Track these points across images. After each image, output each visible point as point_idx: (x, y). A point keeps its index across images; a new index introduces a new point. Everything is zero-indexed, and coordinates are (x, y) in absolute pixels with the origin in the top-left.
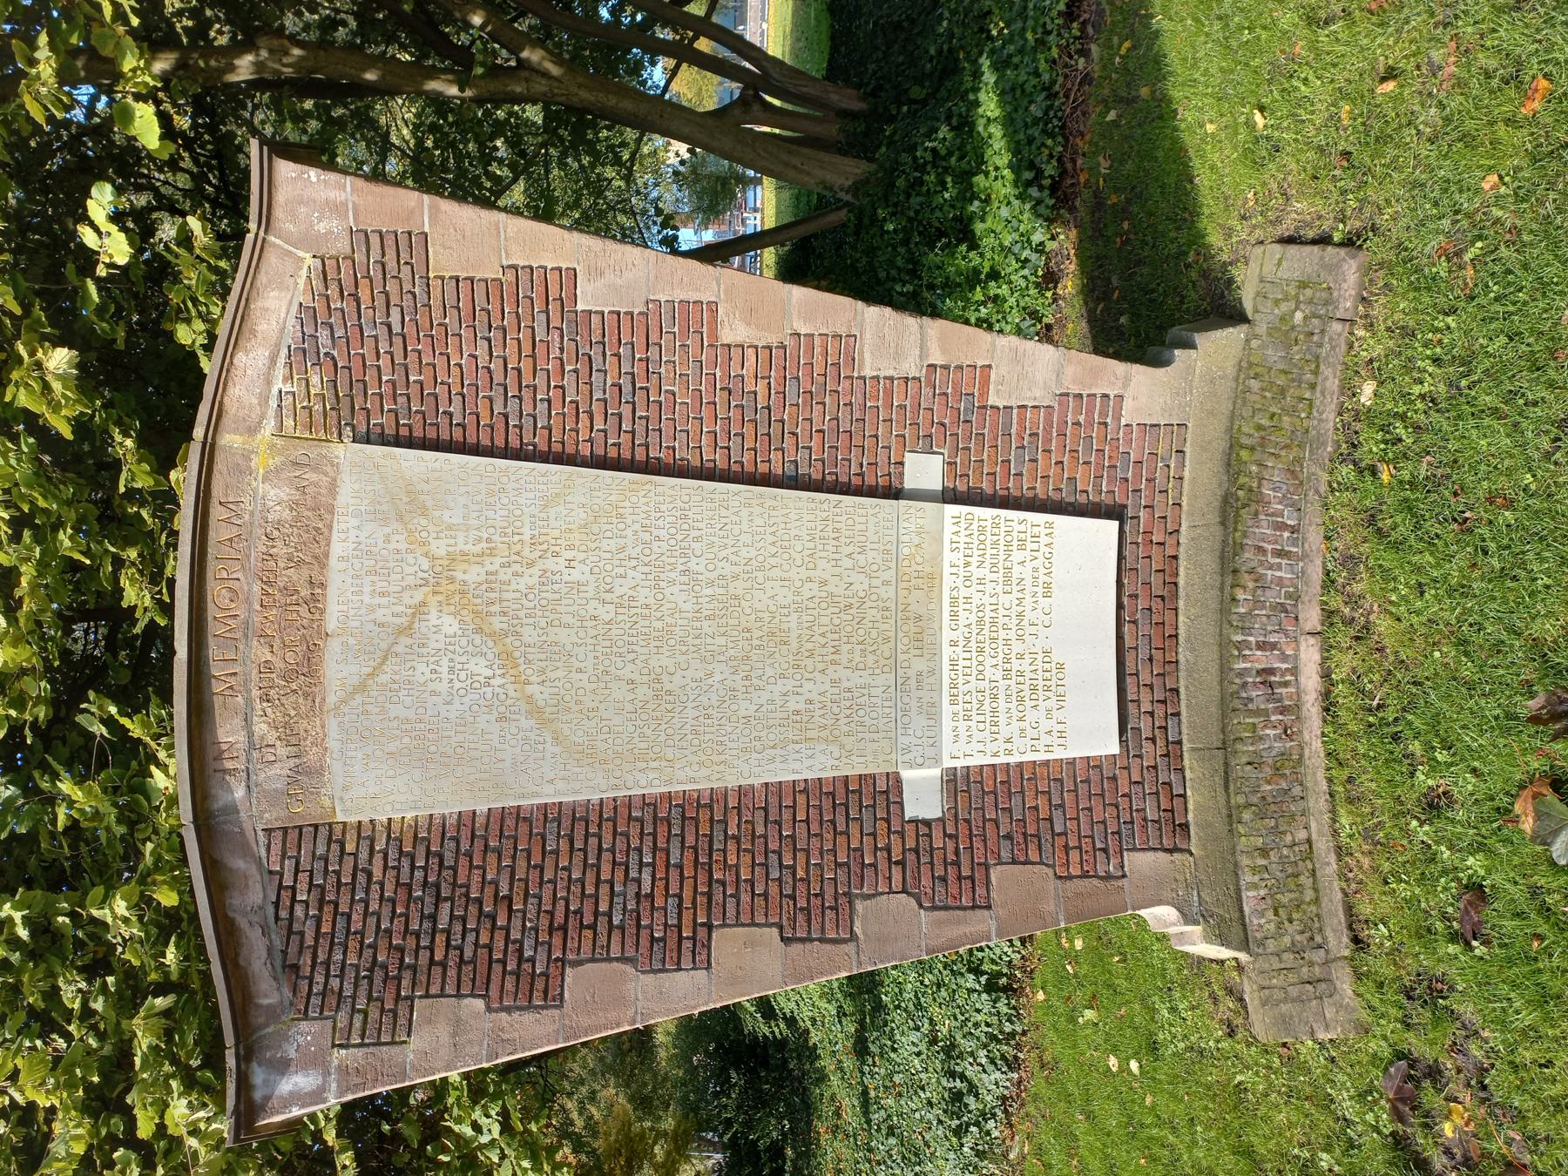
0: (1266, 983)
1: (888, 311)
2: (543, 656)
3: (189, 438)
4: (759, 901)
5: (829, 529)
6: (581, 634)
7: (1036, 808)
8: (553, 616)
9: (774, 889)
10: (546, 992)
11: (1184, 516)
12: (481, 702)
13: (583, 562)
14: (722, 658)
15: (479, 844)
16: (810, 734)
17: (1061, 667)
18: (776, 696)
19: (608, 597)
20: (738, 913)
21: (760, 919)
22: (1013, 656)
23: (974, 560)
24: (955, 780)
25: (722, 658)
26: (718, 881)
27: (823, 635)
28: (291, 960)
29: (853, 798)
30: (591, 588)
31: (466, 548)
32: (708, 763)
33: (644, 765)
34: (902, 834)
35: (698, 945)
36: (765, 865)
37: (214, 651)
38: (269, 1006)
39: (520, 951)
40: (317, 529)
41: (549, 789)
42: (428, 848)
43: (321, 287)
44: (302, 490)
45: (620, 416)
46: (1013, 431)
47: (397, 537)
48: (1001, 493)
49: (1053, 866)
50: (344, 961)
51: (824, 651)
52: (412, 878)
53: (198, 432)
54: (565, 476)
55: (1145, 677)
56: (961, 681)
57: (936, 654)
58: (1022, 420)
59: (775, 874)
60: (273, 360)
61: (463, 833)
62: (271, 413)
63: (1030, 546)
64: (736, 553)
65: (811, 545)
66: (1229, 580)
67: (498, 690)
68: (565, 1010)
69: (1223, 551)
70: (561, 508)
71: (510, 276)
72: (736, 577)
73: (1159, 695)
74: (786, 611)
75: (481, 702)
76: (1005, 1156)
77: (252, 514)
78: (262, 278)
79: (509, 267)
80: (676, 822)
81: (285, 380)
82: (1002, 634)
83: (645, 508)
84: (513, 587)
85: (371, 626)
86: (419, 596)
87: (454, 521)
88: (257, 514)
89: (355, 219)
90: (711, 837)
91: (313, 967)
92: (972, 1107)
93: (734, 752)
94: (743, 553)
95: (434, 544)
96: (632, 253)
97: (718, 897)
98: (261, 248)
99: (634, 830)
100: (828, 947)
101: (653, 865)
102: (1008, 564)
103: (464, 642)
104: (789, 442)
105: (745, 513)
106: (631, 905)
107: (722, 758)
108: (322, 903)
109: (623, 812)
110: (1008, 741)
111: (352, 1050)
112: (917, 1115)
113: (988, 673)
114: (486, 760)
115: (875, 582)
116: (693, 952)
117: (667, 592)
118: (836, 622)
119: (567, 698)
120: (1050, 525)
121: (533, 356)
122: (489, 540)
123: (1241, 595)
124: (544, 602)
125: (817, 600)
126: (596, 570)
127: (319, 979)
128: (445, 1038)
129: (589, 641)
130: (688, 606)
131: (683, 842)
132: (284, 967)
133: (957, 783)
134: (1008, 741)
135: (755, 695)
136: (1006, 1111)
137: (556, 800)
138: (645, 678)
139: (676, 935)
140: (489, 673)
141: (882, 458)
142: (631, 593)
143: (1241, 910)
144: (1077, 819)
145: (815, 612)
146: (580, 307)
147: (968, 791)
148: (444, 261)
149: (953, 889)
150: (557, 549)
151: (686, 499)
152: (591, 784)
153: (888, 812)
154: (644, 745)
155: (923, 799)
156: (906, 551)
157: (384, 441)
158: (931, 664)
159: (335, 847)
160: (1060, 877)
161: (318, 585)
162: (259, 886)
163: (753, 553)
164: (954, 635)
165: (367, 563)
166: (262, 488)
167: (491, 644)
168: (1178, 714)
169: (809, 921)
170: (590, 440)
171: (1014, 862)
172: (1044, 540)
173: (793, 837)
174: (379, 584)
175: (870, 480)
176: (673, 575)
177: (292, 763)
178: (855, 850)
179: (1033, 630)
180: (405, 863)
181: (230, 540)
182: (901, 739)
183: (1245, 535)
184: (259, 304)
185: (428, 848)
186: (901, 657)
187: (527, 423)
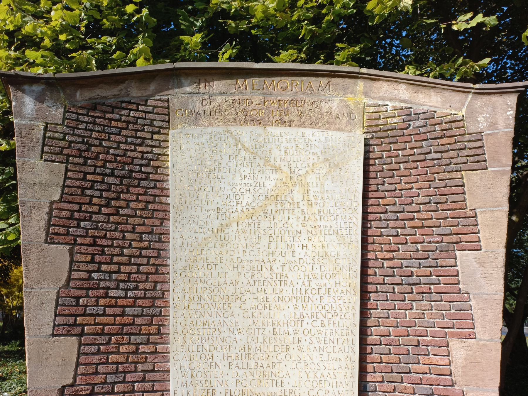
2: (253, 232)
3: (361, 67)
6: (265, 253)
8: (275, 237)
9: (99, 379)
10: (57, 234)
12: (229, 200)
13: (306, 254)
15: (151, 199)
18: (225, 377)
19: (286, 268)
20: (87, 354)
25: (250, 339)
28: (98, 107)
30: (291, 258)
31: (311, 192)
32: (185, 331)
33: (187, 291)
36: (116, 372)
37: (257, 81)
38: (75, 96)
39: (85, 220)
40: (318, 123)
41: (178, 235)
42: (152, 173)
43: (447, 120)
44: (337, 117)
45: (394, 276)
47: (316, 158)
50: (95, 131)
52: (136, 165)
53: (364, 70)
54: (355, 244)
59: (109, 379)
61: (158, 191)
62: (376, 102)
64: (315, 349)
67: (235, 208)
68: (43, 245)
70: (336, 241)
71: (470, 214)
72: (300, 349)
75: (229, 200)
77: (324, 95)
78: (447, 94)
79: (476, 213)
80: (151, 311)
83: (340, 291)
85: (269, 147)
86: (285, 169)
87: (326, 186)
88: (325, 97)
89: (489, 134)
90: (139, 334)
91: (93, 116)
93: (191, 349)
94: (316, 354)
95: (313, 176)
97: (100, 340)
98: (465, 91)
99: (148, 285)
101: (126, 297)
105: (341, 355)
106: (102, 284)
107: (188, 341)
108: (128, 122)
111: (42, 132)
114: (197, 202)
116: (66, 324)
117: (290, 304)
119: (229, 245)
121: (423, 227)
122: (316, 204)
124: (283, 232)
126: (302, 261)
127: (86, 119)
128: (39, 179)
129: (261, 257)
131: (138, 316)
132: (95, 103)
135: (226, 362)
137: (171, 240)
138: (238, 291)
139: (79, 312)
140: (244, 204)
142: (289, 282)
146: (457, 252)
148: (472, 179)
150: (313, 239)
151: (347, 316)
152: (179, 260)
154: (199, 290)
157: (367, 153)
159: (157, 130)
161: (290, 123)
162: (140, 95)
163: (316, 361)
165: (302, 145)
166: (337, 99)
167: (260, 204)
170: (377, 259)
174: (291, 151)
176: (300, 307)
177: (202, 112)
180: (144, 162)
181: (311, 87)
184: (433, 93)
185: (152, 173)
187: (383, 224)
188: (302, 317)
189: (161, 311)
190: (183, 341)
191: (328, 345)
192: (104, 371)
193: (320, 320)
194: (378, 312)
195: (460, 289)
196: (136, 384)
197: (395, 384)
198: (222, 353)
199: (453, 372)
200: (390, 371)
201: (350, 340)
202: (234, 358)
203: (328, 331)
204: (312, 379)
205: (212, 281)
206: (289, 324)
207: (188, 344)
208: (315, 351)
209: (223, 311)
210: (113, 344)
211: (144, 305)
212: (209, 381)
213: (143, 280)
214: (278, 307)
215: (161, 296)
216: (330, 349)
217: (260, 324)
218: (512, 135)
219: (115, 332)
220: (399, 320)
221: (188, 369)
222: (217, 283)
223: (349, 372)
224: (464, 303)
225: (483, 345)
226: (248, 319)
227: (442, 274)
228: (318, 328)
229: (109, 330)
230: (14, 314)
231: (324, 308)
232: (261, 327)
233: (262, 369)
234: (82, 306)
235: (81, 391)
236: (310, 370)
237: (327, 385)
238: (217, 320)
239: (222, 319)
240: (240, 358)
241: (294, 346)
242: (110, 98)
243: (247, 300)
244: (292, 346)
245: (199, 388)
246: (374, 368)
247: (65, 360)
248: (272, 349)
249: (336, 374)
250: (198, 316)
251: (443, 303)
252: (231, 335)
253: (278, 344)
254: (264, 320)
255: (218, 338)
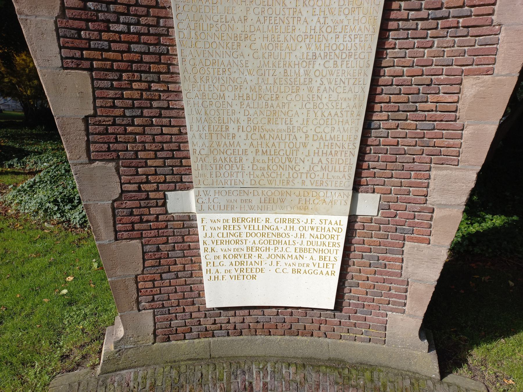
0: (81, 385)
1: (472, 185)
4: (109, 103)
5: (337, 149)
7: (175, 264)
9: (118, 112)
11: (334, 340)
14: (260, 81)
16: (214, 136)
17: (254, 277)
18: (237, 115)
20: (102, 89)
21: (98, 103)
22: (260, 252)
23: (314, 232)
24: (190, 220)
25: (260, 81)
26: (121, 76)
27: (274, 144)
29: (177, 162)
32: (195, 71)
33: (192, 27)
34: (157, 190)
35: (78, 62)
36: (133, 107)
45: (420, 10)
46: (388, 255)
48: (352, 247)
49: (143, 273)
51: (264, 145)
55: (248, 319)
56: (246, 224)
57: (262, 210)
58: (395, 260)
59: (128, 113)
63: (321, 263)
64: (325, 90)
65: (328, 138)
66: (299, 362)
73: (238, 326)
74: (288, 122)
76: (46, 221)
80: (157, 49)
82: (272, 247)
83: (357, 28)
90: (149, 72)
92: (66, 207)
93: (202, 88)
94: (325, 95)
97: (111, 76)
99: (151, 21)
100: (84, 145)
101: (129, 32)
102: (312, 251)
104: (392, 124)
109: (162, 13)
110: (212, 250)
112: (70, 182)
113: (251, 239)
115: (304, 176)
116: (73, 58)
117: (303, 44)
118: (281, 153)
120: (333, 274)
123: (292, 369)
125: (294, 141)
130: (293, 58)
131: (145, 53)
133: (188, 222)
134: (212, 250)
136: (64, 222)
138: (248, 29)
141: (377, 180)
142: (303, 19)
143: (124, 369)
144: (170, 286)
145: (287, 140)
147: (183, 228)
149: (125, 220)
151: (362, 56)
153: (169, 183)
154: (205, 27)
155: (178, 202)
156: (322, 194)
158: (256, 208)
160: (136, 277)
163: (325, 101)
164: (272, 220)
168: (228, 335)
169: (99, 134)
171: (144, 253)
172: (325, 271)
173: (152, 125)
175: (365, 173)
176: (313, 48)
178: (146, 163)
179: (274, 263)
182: (212, 190)
183: (325, 374)
186: (260, 191)
188: (314, 57)
189: (168, 50)
190: (194, 80)
191: (339, 85)
192: (121, 106)
193: (333, 60)
194: (395, 52)
195: (492, 20)
196: (154, 119)
197: (399, 122)
198: (233, 93)
199: (459, 108)
200: (396, 109)
201: (362, 80)
202: (245, 97)
203: (340, 72)
204: (319, 118)
205: (219, 17)
206: (300, 65)
207: (199, 83)
208: (325, 92)
209: (232, 51)
210: (125, 80)
211: (149, 42)
212: (222, 119)
213: (144, 14)
214: (290, 47)
215: (166, 33)
217: (271, 65)
219: (125, 69)
220: (373, 232)
221: (202, 107)
222: (224, 20)
223: (356, 111)
224: (492, 36)
225: (498, 80)
226: (259, 60)
227: (477, 4)
228: (330, 69)
229: (118, 66)
230: (32, 103)
231: (338, 47)
232: (271, 68)
233: (272, 108)
234: (85, 39)
235: (103, 122)
236: (318, 109)
237: (334, 122)
238: (226, 60)
239: (231, 59)
240: (251, 97)
241: (305, 87)
243: (257, 40)
244: (302, 87)
245: (213, 124)
246: (381, 107)
247: (81, 92)
248: (282, 90)
249: (343, 113)
250: (206, 55)
251: (469, 37)
252: (241, 76)
253: (288, 85)
254: (275, 61)
255: (228, 78)
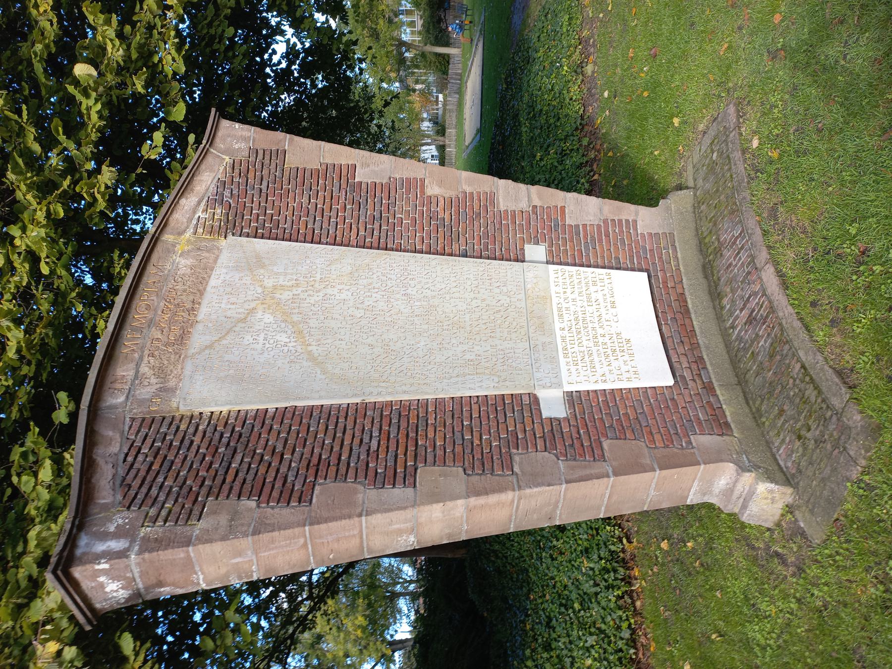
14: (425, 334)
30: (351, 303)
31: (283, 283)
37: (127, 333)
40: (203, 278)
43: (231, 171)
57: (552, 333)
60: (199, 203)
62: (192, 226)
65: (476, 282)
69: (710, 290)
78: (203, 167)
81: (203, 211)
82: (590, 325)
84: (308, 301)
85: (223, 319)
86: (253, 305)
94: (438, 286)
96: (383, 157)
103: (275, 326)
113: (585, 343)
133: (573, 399)
140: (288, 340)
142: (374, 304)
163: (443, 286)
167: (290, 327)
177: (158, 386)
179: (608, 323)
187: (324, 232)
216: (434, 275)
218: (258, 129)
242: (117, 471)
